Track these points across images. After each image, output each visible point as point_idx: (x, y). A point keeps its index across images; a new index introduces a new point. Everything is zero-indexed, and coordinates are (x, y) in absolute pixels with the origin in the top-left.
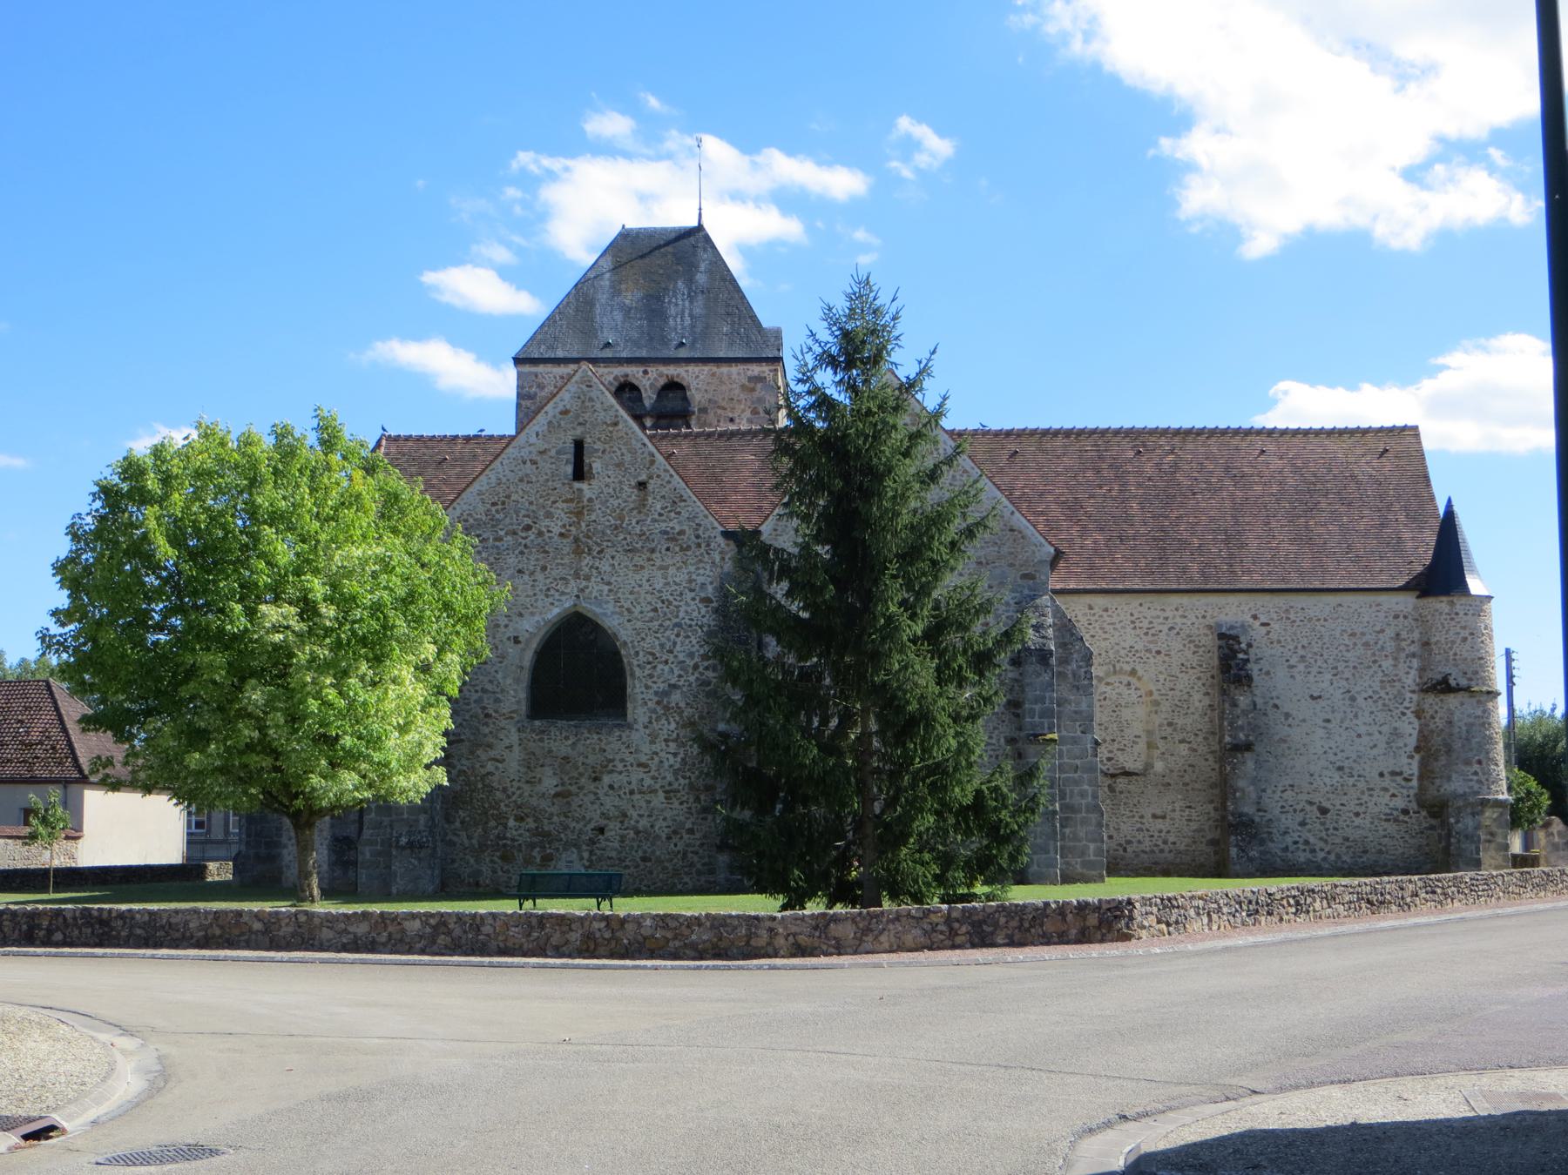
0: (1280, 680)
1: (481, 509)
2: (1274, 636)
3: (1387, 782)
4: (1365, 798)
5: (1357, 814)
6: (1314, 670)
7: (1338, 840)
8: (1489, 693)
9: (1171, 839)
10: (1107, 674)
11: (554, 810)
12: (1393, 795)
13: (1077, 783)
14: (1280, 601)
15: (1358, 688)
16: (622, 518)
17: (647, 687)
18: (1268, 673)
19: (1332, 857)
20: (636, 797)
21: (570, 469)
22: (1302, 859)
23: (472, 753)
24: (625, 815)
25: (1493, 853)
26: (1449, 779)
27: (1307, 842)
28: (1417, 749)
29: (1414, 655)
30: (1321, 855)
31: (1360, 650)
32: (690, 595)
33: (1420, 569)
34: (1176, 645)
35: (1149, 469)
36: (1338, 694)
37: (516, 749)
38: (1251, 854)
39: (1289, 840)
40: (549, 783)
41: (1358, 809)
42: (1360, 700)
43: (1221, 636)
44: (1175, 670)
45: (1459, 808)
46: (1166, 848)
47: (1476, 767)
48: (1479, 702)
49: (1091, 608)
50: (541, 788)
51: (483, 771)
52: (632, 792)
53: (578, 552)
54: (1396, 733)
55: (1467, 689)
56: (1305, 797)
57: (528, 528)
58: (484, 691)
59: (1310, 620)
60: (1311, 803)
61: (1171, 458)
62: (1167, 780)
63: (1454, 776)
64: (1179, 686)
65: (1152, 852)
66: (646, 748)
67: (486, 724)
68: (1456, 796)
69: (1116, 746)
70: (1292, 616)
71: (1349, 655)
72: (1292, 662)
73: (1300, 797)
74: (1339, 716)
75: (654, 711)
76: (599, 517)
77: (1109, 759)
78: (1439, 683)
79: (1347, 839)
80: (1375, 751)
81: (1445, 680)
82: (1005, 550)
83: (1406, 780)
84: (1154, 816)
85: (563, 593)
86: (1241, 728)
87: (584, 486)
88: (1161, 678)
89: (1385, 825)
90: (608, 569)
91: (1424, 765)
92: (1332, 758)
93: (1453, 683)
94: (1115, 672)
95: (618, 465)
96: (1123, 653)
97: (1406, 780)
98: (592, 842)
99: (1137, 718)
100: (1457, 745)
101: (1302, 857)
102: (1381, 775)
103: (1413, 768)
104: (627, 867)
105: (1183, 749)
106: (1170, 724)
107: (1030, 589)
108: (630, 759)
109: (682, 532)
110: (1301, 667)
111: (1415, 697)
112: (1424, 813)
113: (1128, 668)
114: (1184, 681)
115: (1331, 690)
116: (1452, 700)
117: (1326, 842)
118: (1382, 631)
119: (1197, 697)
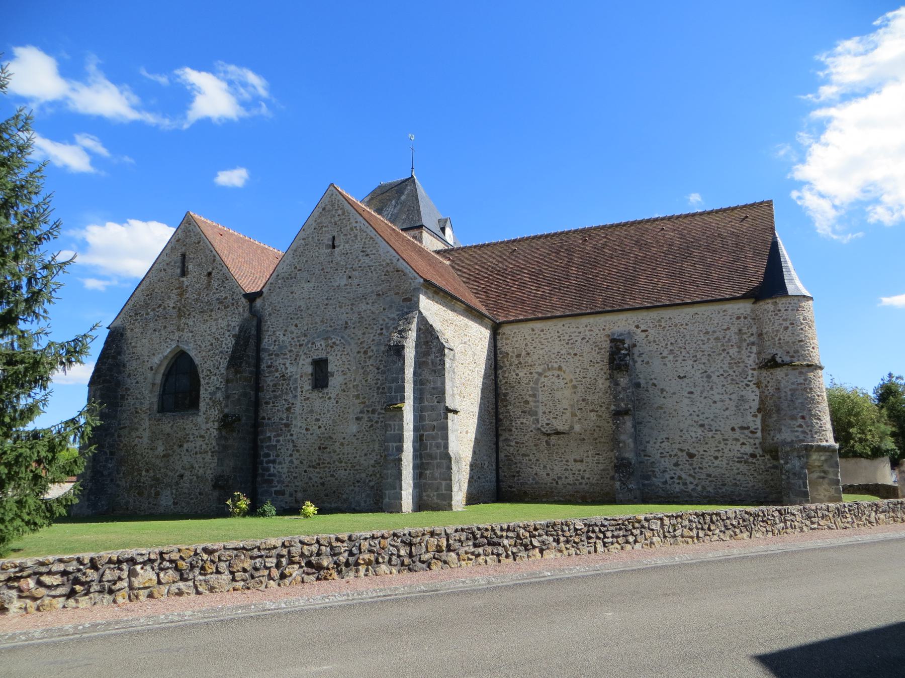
0: (657, 367)
1: (142, 299)
2: (651, 338)
3: (737, 434)
4: (722, 446)
5: (716, 458)
6: (680, 359)
7: (703, 477)
8: (808, 366)
9: (587, 476)
10: (544, 370)
11: (161, 465)
12: (743, 444)
13: (434, 438)
14: (654, 314)
15: (712, 369)
16: (199, 294)
17: (206, 390)
18: (648, 363)
19: (699, 488)
20: (199, 455)
21: (179, 271)
22: (677, 490)
23: (130, 433)
24: (193, 467)
25: (826, 486)
26: (780, 431)
27: (680, 478)
28: (759, 410)
29: (753, 344)
30: (691, 487)
31: (712, 343)
32: (228, 333)
33: (756, 284)
34: (587, 349)
35: (589, 248)
36: (698, 374)
37: (147, 430)
38: (630, 486)
39: (667, 476)
40: (160, 450)
41: (716, 454)
42: (714, 377)
43: (613, 340)
44: (586, 365)
45: (787, 452)
46: (584, 482)
47: (800, 421)
48: (801, 373)
49: (533, 330)
50: (156, 453)
51: (133, 444)
52: (196, 453)
53: (179, 317)
54: (742, 399)
55: (789, 364)
56: (678, 446)
57: (160, 306)
58: (137, 398)
59: (676, 325)
60: (682, 450)
61: (604, 240)
62: (583, 436)
63: (783, 428)
64: (589, 375)
65: (575, 484)
66: (204, 427)
67: (136, 417)
68: (784, 443)
69: (552, 416)
70: (663, 324)
71: (703, 347)
72: (664, 354)
73: (674, 446)
74: (699, 389)
75: (208, 404)
76: (191, 295)
77: (548, 424)
78: (769, 361)
79: (709, 476)
80: (727, 413)
81: (773, 359)
82: (394, 284)
83: (752, 432)
84: (575, 461)
85: (172, 340)
86: (623, 400)
87: (184, 279)
88: (578, 370)
89: (738, 465)
90: (192, 323)
91: (763, 421)
92: (696, 418)
93: (779, 360)
94: (549, 369)
95: (199, 265)
96: (553, 356)
97: (752, 432)
98: (177, 483)
99: (566, 397)
100: (784, 405)
101: (678, 488)
102: (733, 429)
103: (756, 423)
104: (192, 499)
105: (593, 416)
106: (584, 400)
107: (408, 308)
108: (196, 433)
109: (226, 298)
110: (671, 357)
111: (755, 373)
112: (768, 457)
113: (556, 365)
114: (592, 372)
115: (693, 371)
116: (779, 373)
117: (694, 477)
118: (729, 328)
119: (600, 381)
